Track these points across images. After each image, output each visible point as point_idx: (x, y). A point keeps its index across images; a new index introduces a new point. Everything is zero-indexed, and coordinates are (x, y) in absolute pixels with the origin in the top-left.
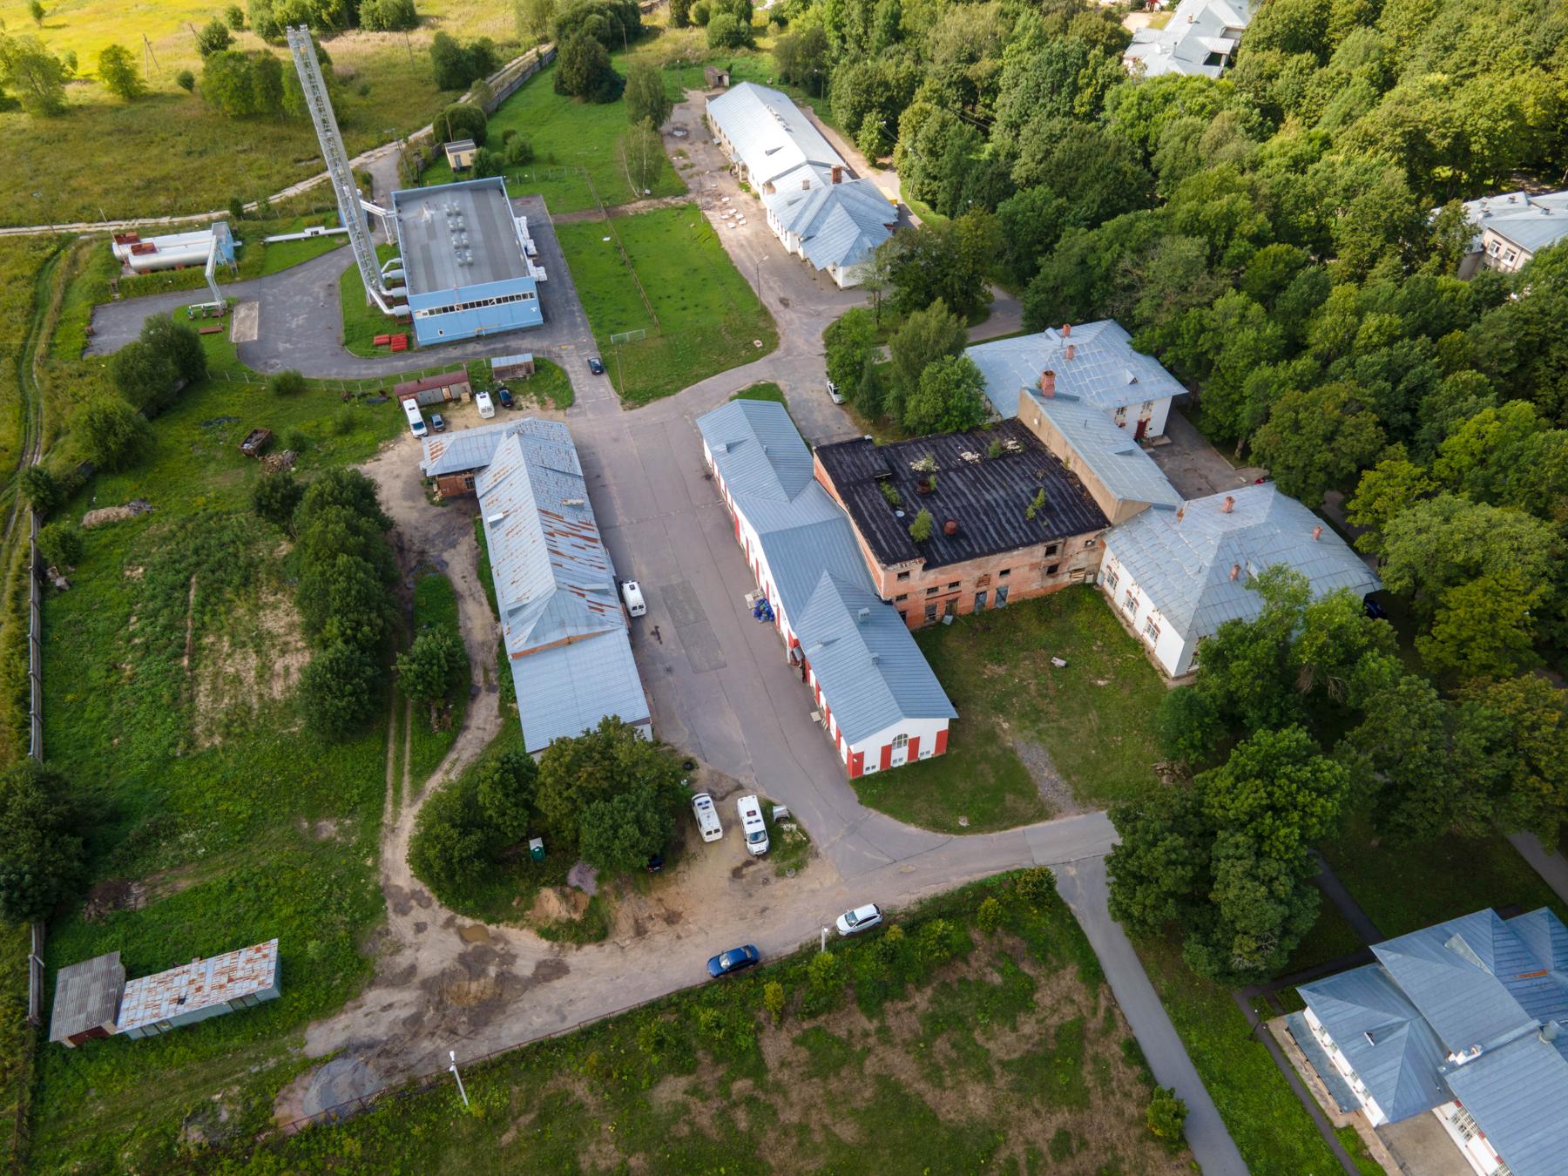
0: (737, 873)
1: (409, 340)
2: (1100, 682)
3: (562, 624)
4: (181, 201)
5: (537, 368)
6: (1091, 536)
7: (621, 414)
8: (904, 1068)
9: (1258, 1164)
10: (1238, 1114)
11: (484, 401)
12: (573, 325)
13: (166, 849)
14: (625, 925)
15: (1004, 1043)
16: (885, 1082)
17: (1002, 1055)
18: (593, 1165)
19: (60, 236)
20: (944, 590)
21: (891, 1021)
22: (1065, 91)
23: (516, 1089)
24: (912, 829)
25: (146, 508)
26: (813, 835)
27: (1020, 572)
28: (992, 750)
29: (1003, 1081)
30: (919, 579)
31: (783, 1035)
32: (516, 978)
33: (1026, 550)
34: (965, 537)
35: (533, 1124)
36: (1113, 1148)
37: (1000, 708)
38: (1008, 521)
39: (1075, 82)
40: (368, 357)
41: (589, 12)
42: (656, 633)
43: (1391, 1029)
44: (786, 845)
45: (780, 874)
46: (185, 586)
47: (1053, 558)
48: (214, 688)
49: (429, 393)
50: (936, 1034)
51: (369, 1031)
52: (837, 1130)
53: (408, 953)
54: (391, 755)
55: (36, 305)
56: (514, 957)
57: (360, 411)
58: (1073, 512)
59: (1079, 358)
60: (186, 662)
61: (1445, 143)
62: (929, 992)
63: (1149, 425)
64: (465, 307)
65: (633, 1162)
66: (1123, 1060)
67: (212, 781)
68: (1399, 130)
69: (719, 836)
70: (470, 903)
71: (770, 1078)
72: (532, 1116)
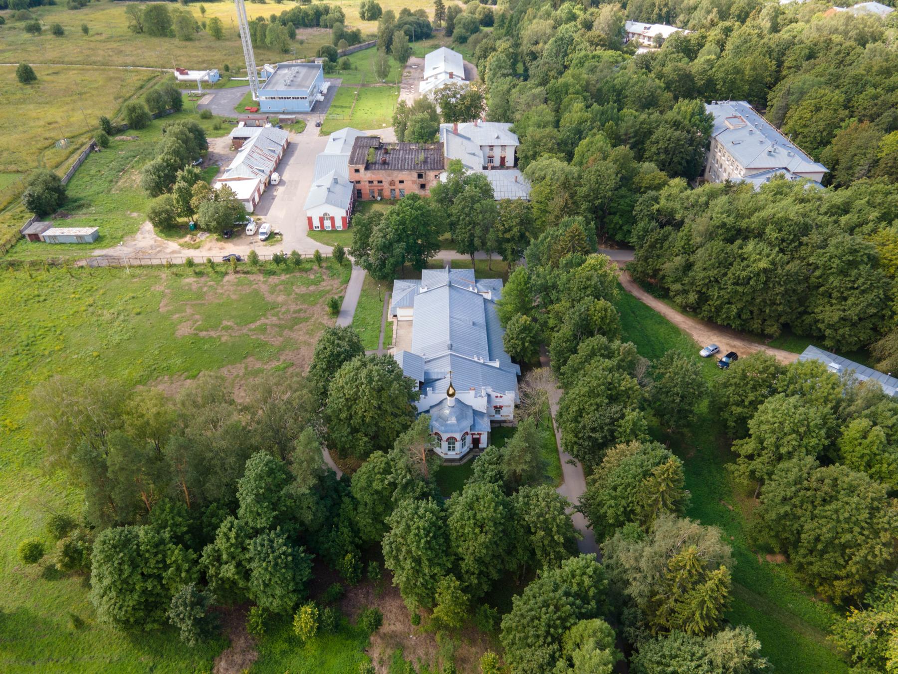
6: (436, 173)
13: (84, 211)
20: (376, 183)
30: (365, 176)
39: (566, 51)
40: (240, 113)
41: (406, 24)
45: (266, 246)
46: (135, 157)
47: (422, 181)
55: (141, 88)
61: (702, 82)
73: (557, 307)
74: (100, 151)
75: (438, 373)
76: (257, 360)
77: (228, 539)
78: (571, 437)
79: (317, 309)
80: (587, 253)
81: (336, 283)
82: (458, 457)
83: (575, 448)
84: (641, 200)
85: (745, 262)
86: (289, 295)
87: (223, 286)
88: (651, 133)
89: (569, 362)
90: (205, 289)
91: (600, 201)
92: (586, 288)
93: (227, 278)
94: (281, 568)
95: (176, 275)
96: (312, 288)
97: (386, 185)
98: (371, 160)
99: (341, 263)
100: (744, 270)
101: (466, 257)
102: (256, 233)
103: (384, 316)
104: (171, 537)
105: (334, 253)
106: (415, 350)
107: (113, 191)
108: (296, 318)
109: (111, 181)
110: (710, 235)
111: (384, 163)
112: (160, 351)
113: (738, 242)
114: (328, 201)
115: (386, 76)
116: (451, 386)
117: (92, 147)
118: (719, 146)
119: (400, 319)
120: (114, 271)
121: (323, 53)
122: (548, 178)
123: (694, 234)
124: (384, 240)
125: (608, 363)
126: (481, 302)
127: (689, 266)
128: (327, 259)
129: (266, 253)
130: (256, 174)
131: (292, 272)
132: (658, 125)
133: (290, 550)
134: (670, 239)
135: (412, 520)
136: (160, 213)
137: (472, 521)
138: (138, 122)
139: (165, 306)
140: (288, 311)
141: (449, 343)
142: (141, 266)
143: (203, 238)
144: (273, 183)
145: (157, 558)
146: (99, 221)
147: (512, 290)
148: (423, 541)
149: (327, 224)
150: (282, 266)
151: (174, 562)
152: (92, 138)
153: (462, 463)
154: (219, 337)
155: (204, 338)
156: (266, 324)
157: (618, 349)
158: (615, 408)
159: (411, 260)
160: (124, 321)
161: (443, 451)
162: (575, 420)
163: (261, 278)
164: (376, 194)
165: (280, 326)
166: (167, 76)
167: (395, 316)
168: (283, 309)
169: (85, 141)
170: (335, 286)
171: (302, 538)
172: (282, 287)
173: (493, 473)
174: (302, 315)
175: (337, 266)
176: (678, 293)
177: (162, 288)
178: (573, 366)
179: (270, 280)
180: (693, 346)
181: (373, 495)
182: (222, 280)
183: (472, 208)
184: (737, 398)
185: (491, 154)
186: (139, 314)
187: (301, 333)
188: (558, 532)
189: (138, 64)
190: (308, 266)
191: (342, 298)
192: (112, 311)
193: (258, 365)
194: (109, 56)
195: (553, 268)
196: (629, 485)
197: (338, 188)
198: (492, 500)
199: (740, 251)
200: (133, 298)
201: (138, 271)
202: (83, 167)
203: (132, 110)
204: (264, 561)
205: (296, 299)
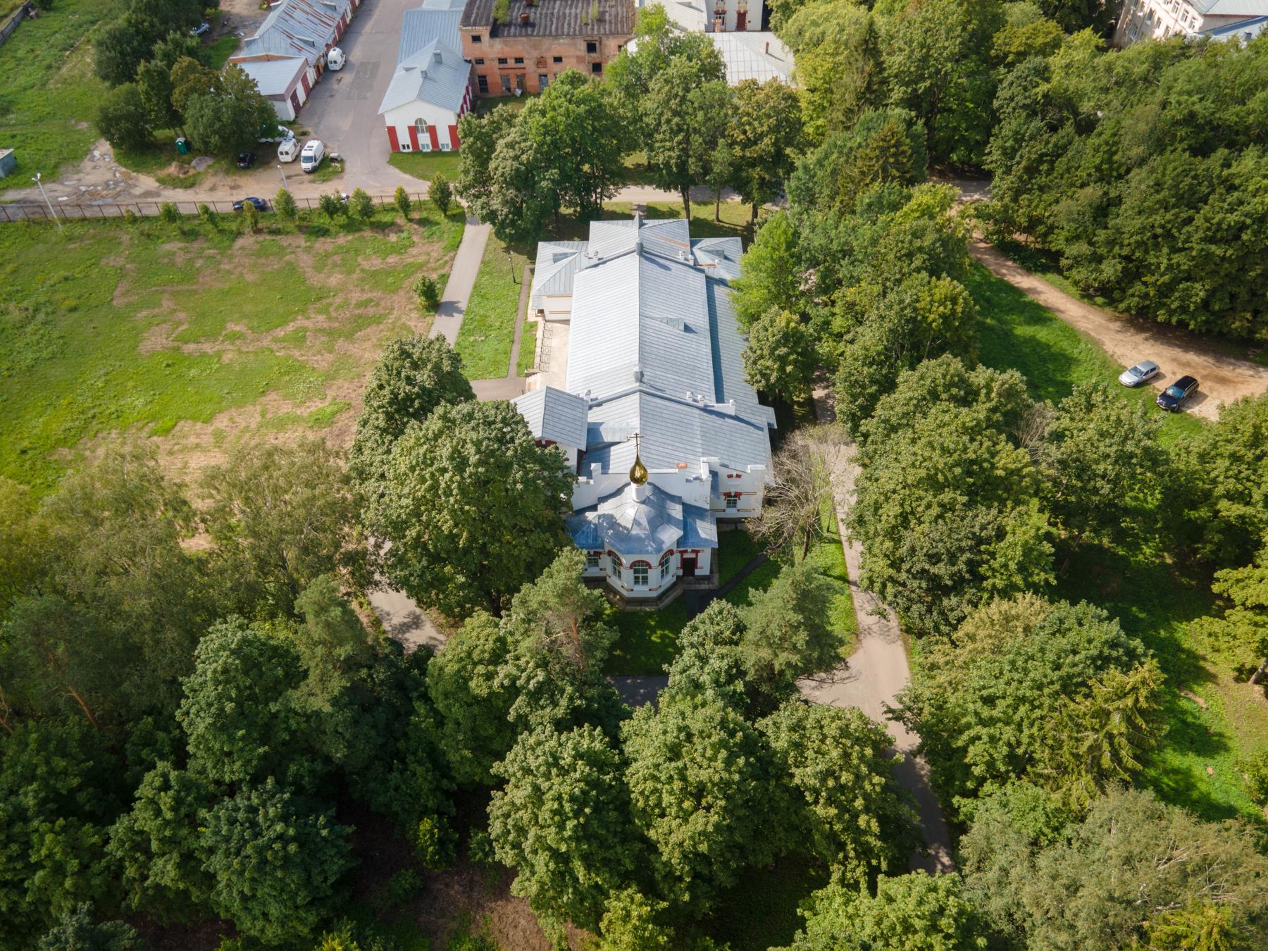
20: (511, 63)
24: (407, 176)
30: (492, 49)
38: (569, 24)
45: (313, 182)
46: (93, 23)
47: (595, 57)
53: (81, 175)
58: (616, 24)
65: (128, 266)
73: (850, 293)
74: (37, 16)
75: (614, 432)
76: (285, 398)
77: (158, 812)
78: (881, 566)
79: (399, 299)
80: (911, 182)
81: (436, 249)
82: (654, 594)
83: (890, 589)
84: (1010, 77)
85: (1236, 194)
86: (349, 273)
87: (232, 257)
89: (879, 411)
90: (199, 263)
91: (928, 83)
92: (910, 255)
93: (240, 242)
94: (275, 868)
95: (149, 236)
96: (392, 259)
97: (529, 65)
99: (445, 211)
100: (1232, 211)
101: (673, 198)
102: (297, 159)
103: (520, 313)
104: (42, 803)
105: (433, 192)
106: (572, 385)
107: (51, 85)
108: (360, 316)
109: (49, 67)
110: (1159, 142)
111: (526, 23)
112: (107, 382)
113: (1222, 152)
114: (422, 96)
116: (638, 463)
117: (26, 11)
119: (549, 317)
120: (36, 230)
122: (829, 38)
123: (1126, 141)
124: (516, 164)
125: (968, 416)
126: (700, 281)
127: (1102, 211)
128: (421, 205)
129: (309, 195)
130: (300, 49)
131: (360, 230)
133: (291, 832)
134: (1070, 154)
135: (548, 776)
136: (117, 119)
137: (677, 785)
139: (124, 295)
140: (347, 303)
141: (637, 369)
142: (84, 219)
143: (202, 168)
145: (8, 852)
146: (19, 138)
147: (761, 259)
148: (570, 824)
149: (424, 139)
150: (341, 219)
151: (47, 856)
153: (661, 605)
154: (219, 354)
155: (190, 354)
156: (305, 329)
157: (988, 387)
158: (984, 516)
159: (571, 204)
160: (45, 323)
161: (624, 583)
162: (893, 534)
163: (302, 241)
165: (330, 333)
167: (541, 312)
168: (338, 300)
170: (434, 255)
171: (333, 791)
172: (337, 258)
173: (724, 664)
174: (371, 311)
175: (439, 216)
176: (1077, 261)
177: (121, 261)
178: (886, 421)
179: (317, 245)
180: (1105, 364)
181: (469, 705)
182: (230, 247)
183: (683, 99)
184: (1231, 484)
186: (74, 309)
187: (368, 345)
188: (867, 810)
190: (387, 218)
191: (445, 278)
192: (25, 304)
193: (286, 408)
195: (842, 214)
196: (1023, 700)
197: (444, 74)
198: (722, 744)
199: (1226, 172)
200: (66, 279)
201: (79, 230)
202: (7, 46)
204: (238, 853)
205: (363, 279)
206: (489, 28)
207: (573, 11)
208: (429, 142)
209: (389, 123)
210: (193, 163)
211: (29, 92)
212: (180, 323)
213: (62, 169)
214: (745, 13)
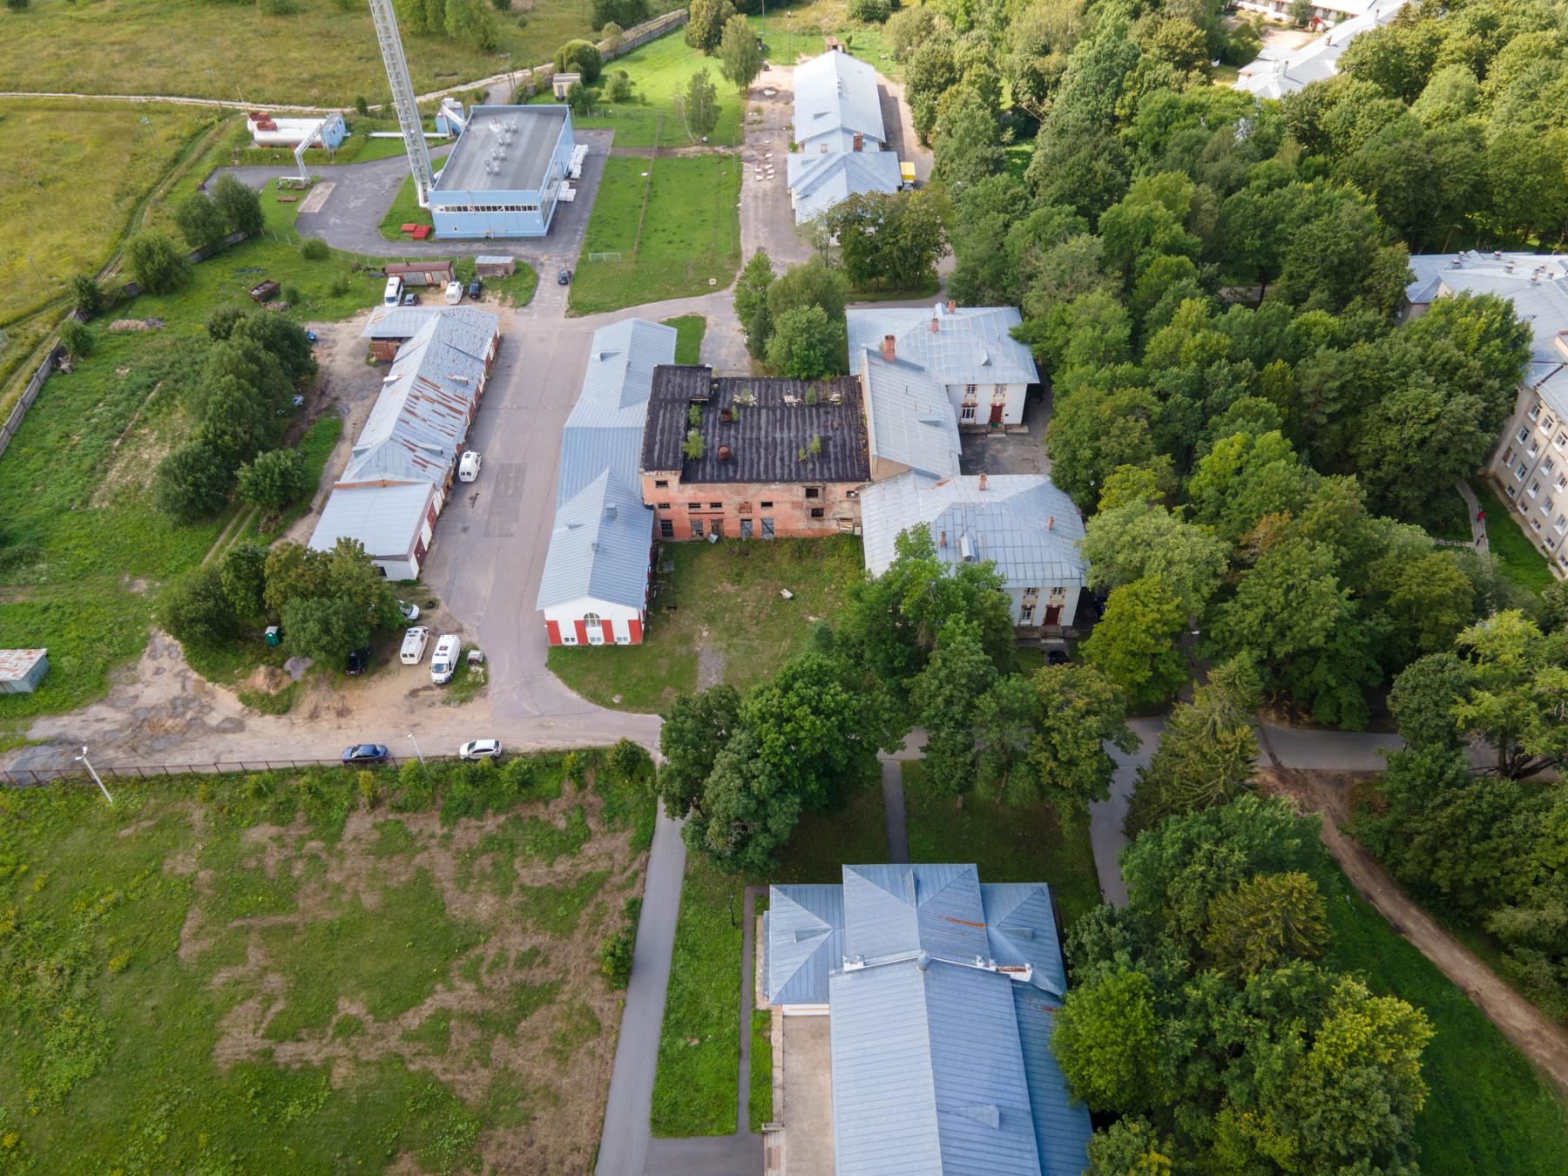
0: (414, 693)
1: (431, 231)
2: (811, 618)
3: (385, 470)
4: (330, 96)
5: (516, 271)
6: (852, 486)
7: (561, 320)
8: (444, 865)
9: (673, 1016)
10: (683, 976)
11: (453, 289)
12: (571, 242)
13: (22, 573)
14: (306, 708)
15: (534, 873)
16: (424, 878)
17: (527, 882)
18: (173, 868)
19: (224, 110)
20: (706, 508)
21: (458, 833)
22: (1109, 91)
23: (152, 801)
24: (573, 695)
25: (160, 324)
26: (492, 681)
27: (783, 507)
28: (681, 650)
29: (514, 899)
30: (678, 494)
31: (370, 818)
32: (204, 724)
33: (783, 486)
34: (735, 463)
35: (150, 829)
36: (567, 972)
37: (710, 619)
38: (782, 459)
39: (1120, 82)
40: (392, 240)
42: (474, 499)
43: (814, 933)
44: (465, 678)
45: (446, 702)
46: (150, 388)
47: (815, 502)
48: (127, 467)
49: (413, 275)
50: (485, 851)
51: (77, 733)
52: (363, 897)
53: (139, 686)
54: (218, 544)
55: (176, 160)
56: (212, 709)
57: (355, 282)
58: (844, 462)
59: (944, 333)
60: (117, 443)
62: (502, 819)
63: (1004, 411)
64: (477, 209)
65: (201, 875)
66: (621, 912)
67: (82, 532)
68: (1403, 168)
69: (415, 661)
70: (204, 663)
71: (339, 846)
72: (151, 823)
86: (506, 892)
88: (1380, 391)
98: (694, 450)
103: (745, 990)
114: (596, 591)
115: (710, 129)
118: (1544, 413)
121: (571, 61)
126: (1007, 988)
132: (1404, 375)
138: (162, 279)
144: (464, 478)
152: (63, 315)
164: (707, 528)
166: (232, 128)
169: (42, 332)
185: (970, 399)
189: (171, 87)
194: (114, 65)
203: (146, 254)
206: (679, 473)
207: (785, 435)
208: (601, 636)
209: (549, 617)
210: (287, 666)
211: (65, 517)
212: (270, 999)
213: (113, 675)
214: (1001, 407)
